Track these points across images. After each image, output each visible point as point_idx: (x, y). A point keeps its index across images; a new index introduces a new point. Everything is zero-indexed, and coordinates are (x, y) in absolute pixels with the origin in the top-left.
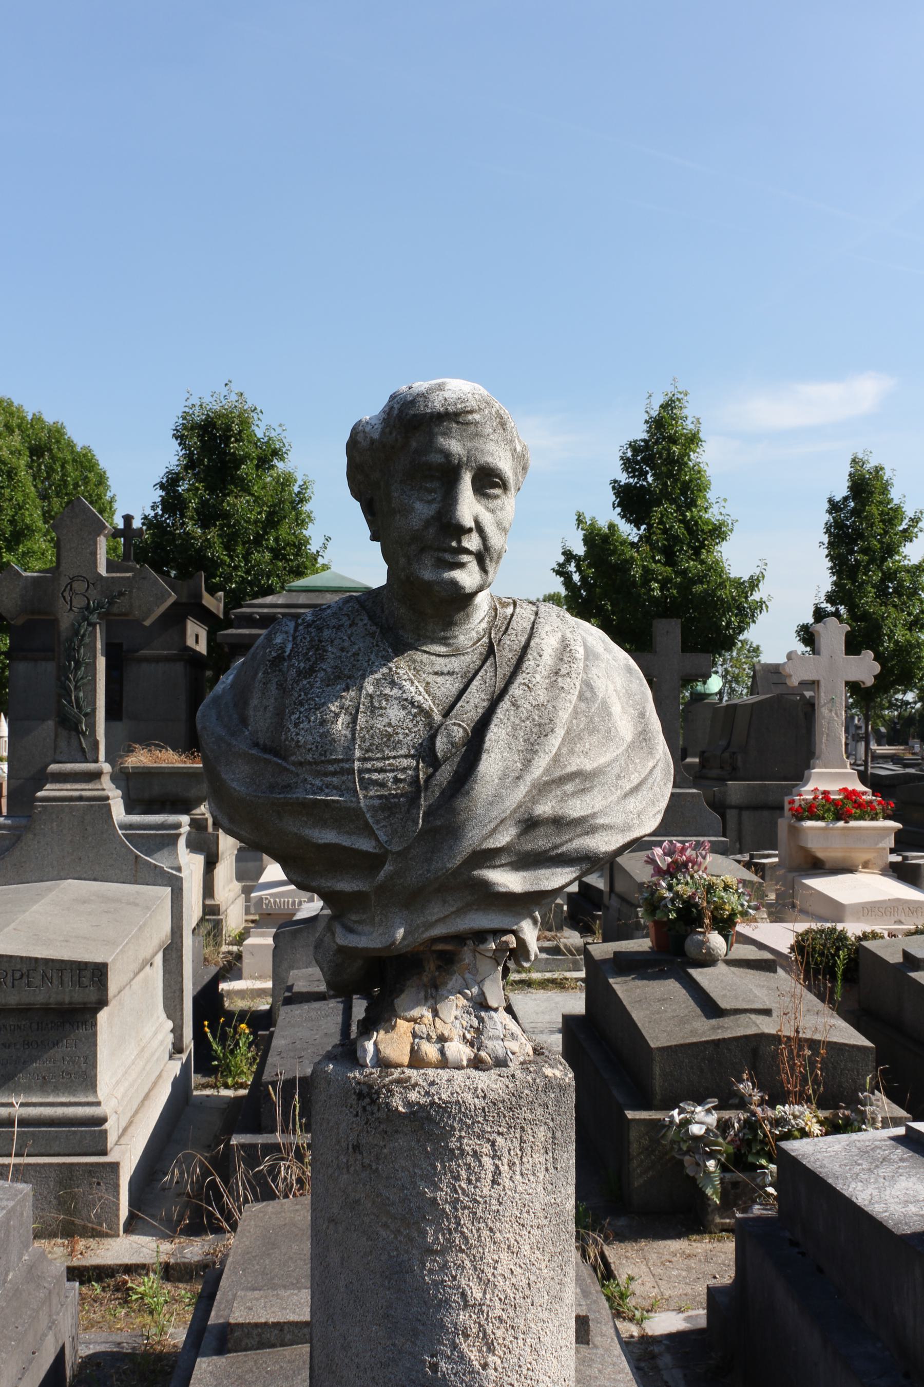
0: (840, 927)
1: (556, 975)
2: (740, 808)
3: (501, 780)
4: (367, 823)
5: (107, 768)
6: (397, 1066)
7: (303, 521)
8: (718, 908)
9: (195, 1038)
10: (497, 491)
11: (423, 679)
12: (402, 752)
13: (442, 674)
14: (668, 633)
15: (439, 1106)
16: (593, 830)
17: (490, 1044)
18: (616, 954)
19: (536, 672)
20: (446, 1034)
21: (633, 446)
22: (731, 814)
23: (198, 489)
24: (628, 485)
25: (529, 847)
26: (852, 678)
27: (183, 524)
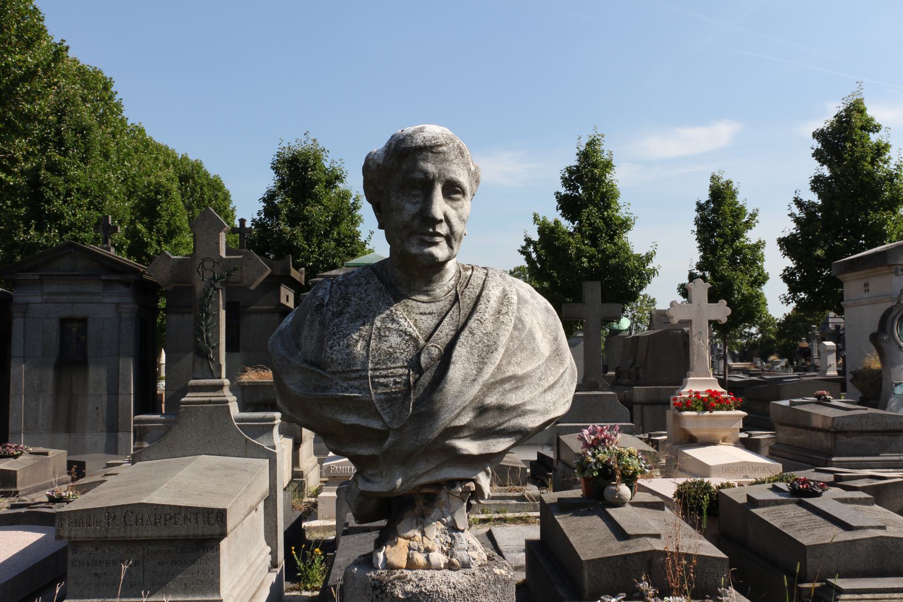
0: (706, 480)
1: (523, 515)
2: (642, 404)
3: (462, 380)
4: (377, 411)
5: (227, 382)
6: (398, 568)
7: (356, 221)
8: (626, 468)
9: (285, 558)
10: (458, 196)
11: (412, 317)
12: (399, 365)
13: (425, 314)
14: (593, 291)
15: (425, 594)
16: (524, 413)
17: (459, 553)
18: (560, 499)
19: (485, 312)
20: (430, 547)
21: (569, 170)
22: (637, 408)
23: (287, 201)
24: (566, 195)
25: (482, 425)
26: (713, 317)
27: (278, 224)
